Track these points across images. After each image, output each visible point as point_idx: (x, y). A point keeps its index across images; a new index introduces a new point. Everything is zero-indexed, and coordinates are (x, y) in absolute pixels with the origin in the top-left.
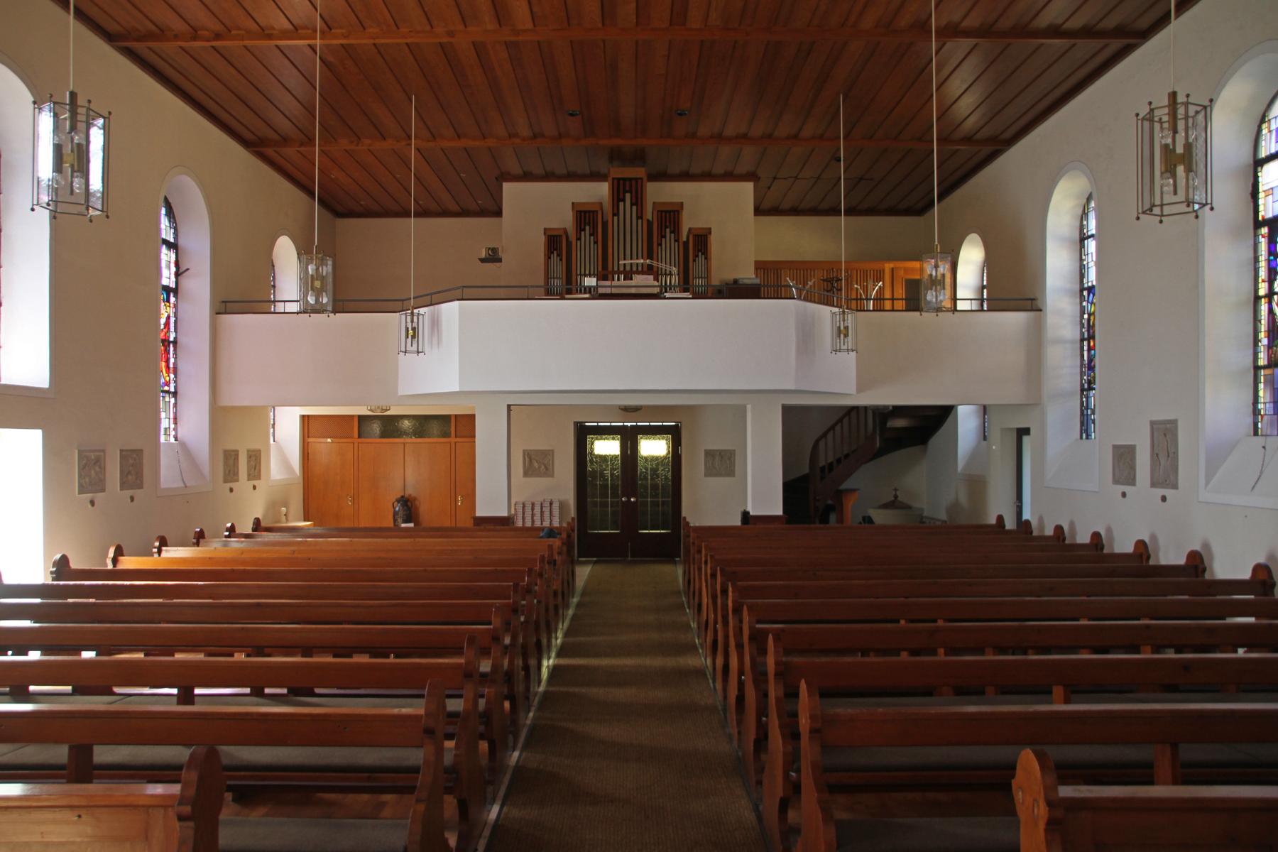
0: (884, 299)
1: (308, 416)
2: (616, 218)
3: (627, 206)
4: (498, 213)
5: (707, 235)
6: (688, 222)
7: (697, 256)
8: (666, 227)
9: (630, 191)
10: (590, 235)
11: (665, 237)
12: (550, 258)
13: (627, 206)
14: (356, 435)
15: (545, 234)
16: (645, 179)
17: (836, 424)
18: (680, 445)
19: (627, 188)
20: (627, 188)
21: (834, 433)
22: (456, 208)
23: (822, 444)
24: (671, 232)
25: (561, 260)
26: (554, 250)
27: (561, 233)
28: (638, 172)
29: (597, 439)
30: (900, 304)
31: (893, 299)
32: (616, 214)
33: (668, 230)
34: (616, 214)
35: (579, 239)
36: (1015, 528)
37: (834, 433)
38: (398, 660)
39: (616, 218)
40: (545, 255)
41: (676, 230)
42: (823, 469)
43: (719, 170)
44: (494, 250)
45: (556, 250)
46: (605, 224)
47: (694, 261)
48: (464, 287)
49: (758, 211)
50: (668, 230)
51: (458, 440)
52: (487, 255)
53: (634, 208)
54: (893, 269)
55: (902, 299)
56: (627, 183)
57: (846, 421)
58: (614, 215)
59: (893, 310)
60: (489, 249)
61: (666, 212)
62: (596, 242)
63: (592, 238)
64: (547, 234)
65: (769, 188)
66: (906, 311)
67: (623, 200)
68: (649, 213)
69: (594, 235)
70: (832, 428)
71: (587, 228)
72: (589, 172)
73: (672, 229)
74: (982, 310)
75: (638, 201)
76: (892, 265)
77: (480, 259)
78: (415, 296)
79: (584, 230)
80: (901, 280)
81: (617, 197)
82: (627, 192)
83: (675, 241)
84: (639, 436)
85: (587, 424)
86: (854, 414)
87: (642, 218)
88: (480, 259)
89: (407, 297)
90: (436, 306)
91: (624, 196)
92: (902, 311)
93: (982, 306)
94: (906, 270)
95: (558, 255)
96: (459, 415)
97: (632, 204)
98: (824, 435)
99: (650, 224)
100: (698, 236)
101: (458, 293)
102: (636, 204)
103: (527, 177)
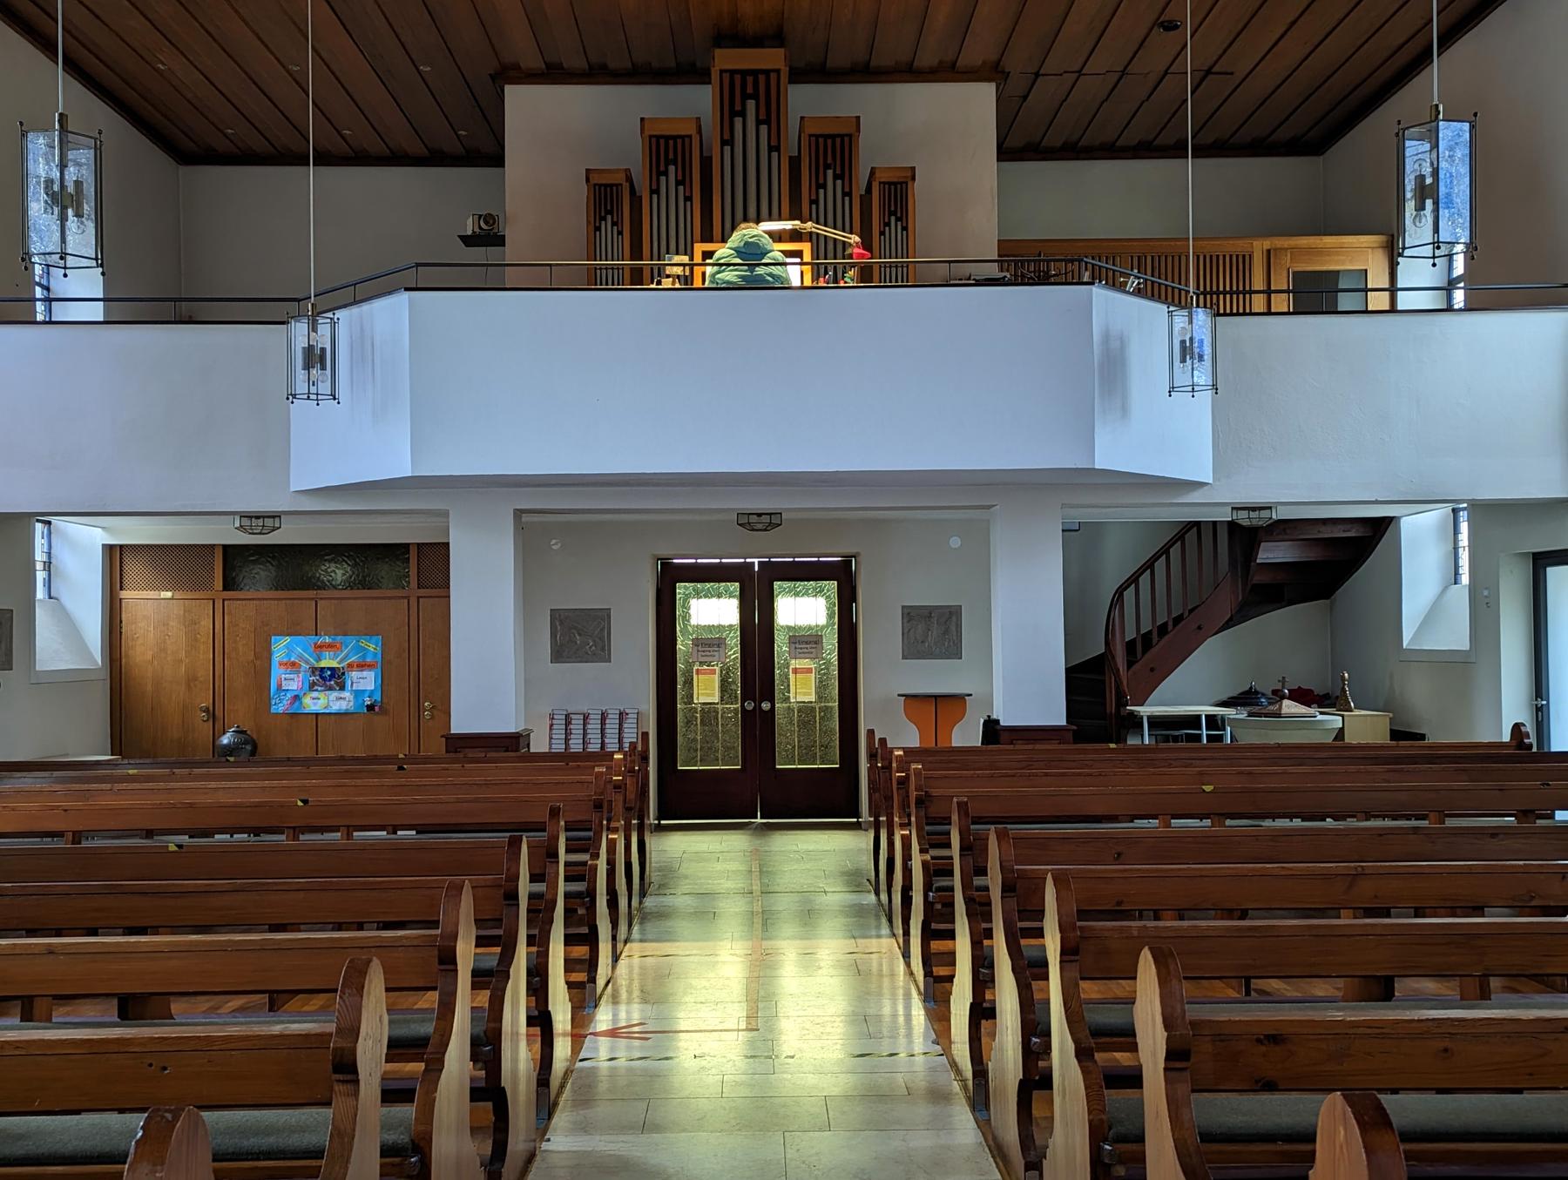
0: (1251, 292)
1: (121, 546)
2: (727, 149)
3: (748, 127)
4: (498, 160)
5: (906, 183)
6: (871, 156)
7: (888, 224)
8: (827, 167)
9: (755, 96)
10: (678, 183)
11: (824, 186)
12: (598, 229)
13: (748, 127)
14: (219, 583)
15: (588, 180)
16: (784, 78)
17: (1155, 558)
18: (855, 600)
19: (750, 90)
20: (750, 90)
21: (1153, 574)
22: (417, 148)
23: (1129, 594)
24: (836, 177)
25: (620, 233)
26: (608, 212)
27: (620, 178)
28: (771, 58)
29: (698, 595)
30: (1281, 302)
31: (1268, 292)
32: (728, 142)
33: (830, 173)
34: (728, 142)
35: (655, 191)
36: (1549, 569)
37: (1153, 574)
38: (191, 840)
39: (727, 149)
40: (588, 222)
41: (845, 172)
42: (1130, 646)
43: (926, 59)
44: (489, 219)
45: (611, 212)
46: (706, 163)
47: (882, 233)
48: (418, 265)
49: (1005, 153)
50: (830, 173)
51: (422, 592)
52: (477, 230)
53: (764, 128)
54: (1269, 251)
55: (1288, 291)
56: (750, 79)
57: (1175, 551)
58: (724, 143)
59: (1269, 313)
60: (480, 216)
61: (826, 137)
62: (688, 198)
63: (681, 188)
64: (592, 182)
65: (1025, 98)
66: (1294, 313)
67: (743, 114)
68: (790, 144)
69: (684, 185)
70: (1149, 565)
71: (672, 168)
72: (673, 65)
73: (838, 172)
74: (1449, 309)
75: (771, 116)
76: (1267, 244)
77: (461, 237)
78: (322, 289)
79: (666, 173)
80: (1285, 274)
81: (730, 110)
82: (750, 97)
83: (844, 194)
84: (777, 584)
85: (674, 561)
86: (1191, 536)
87: (778, 149)
88: (461, 237)
89: (306, 295)
90: (365, 307)
91: (744, 105)
92: (1288, 313)
93: (1450, 298)
94: (1297, 252)
95: (614, 224)
96: (423, 544)
97: (759, 122)
98: (1134, 580)
99: (795, 163)
100: (890, 184)
101: (410, 277)
102: (767, 122)
103: (553, 74)
